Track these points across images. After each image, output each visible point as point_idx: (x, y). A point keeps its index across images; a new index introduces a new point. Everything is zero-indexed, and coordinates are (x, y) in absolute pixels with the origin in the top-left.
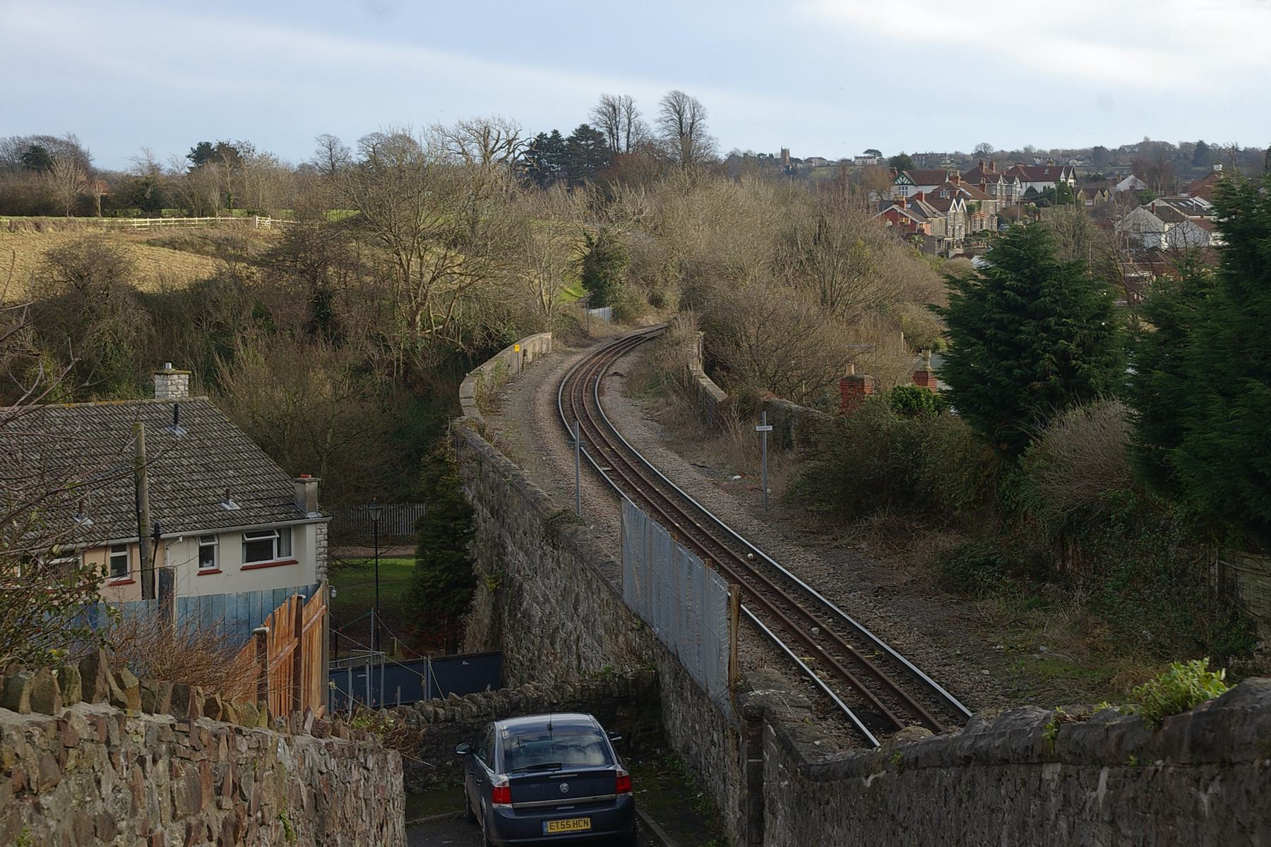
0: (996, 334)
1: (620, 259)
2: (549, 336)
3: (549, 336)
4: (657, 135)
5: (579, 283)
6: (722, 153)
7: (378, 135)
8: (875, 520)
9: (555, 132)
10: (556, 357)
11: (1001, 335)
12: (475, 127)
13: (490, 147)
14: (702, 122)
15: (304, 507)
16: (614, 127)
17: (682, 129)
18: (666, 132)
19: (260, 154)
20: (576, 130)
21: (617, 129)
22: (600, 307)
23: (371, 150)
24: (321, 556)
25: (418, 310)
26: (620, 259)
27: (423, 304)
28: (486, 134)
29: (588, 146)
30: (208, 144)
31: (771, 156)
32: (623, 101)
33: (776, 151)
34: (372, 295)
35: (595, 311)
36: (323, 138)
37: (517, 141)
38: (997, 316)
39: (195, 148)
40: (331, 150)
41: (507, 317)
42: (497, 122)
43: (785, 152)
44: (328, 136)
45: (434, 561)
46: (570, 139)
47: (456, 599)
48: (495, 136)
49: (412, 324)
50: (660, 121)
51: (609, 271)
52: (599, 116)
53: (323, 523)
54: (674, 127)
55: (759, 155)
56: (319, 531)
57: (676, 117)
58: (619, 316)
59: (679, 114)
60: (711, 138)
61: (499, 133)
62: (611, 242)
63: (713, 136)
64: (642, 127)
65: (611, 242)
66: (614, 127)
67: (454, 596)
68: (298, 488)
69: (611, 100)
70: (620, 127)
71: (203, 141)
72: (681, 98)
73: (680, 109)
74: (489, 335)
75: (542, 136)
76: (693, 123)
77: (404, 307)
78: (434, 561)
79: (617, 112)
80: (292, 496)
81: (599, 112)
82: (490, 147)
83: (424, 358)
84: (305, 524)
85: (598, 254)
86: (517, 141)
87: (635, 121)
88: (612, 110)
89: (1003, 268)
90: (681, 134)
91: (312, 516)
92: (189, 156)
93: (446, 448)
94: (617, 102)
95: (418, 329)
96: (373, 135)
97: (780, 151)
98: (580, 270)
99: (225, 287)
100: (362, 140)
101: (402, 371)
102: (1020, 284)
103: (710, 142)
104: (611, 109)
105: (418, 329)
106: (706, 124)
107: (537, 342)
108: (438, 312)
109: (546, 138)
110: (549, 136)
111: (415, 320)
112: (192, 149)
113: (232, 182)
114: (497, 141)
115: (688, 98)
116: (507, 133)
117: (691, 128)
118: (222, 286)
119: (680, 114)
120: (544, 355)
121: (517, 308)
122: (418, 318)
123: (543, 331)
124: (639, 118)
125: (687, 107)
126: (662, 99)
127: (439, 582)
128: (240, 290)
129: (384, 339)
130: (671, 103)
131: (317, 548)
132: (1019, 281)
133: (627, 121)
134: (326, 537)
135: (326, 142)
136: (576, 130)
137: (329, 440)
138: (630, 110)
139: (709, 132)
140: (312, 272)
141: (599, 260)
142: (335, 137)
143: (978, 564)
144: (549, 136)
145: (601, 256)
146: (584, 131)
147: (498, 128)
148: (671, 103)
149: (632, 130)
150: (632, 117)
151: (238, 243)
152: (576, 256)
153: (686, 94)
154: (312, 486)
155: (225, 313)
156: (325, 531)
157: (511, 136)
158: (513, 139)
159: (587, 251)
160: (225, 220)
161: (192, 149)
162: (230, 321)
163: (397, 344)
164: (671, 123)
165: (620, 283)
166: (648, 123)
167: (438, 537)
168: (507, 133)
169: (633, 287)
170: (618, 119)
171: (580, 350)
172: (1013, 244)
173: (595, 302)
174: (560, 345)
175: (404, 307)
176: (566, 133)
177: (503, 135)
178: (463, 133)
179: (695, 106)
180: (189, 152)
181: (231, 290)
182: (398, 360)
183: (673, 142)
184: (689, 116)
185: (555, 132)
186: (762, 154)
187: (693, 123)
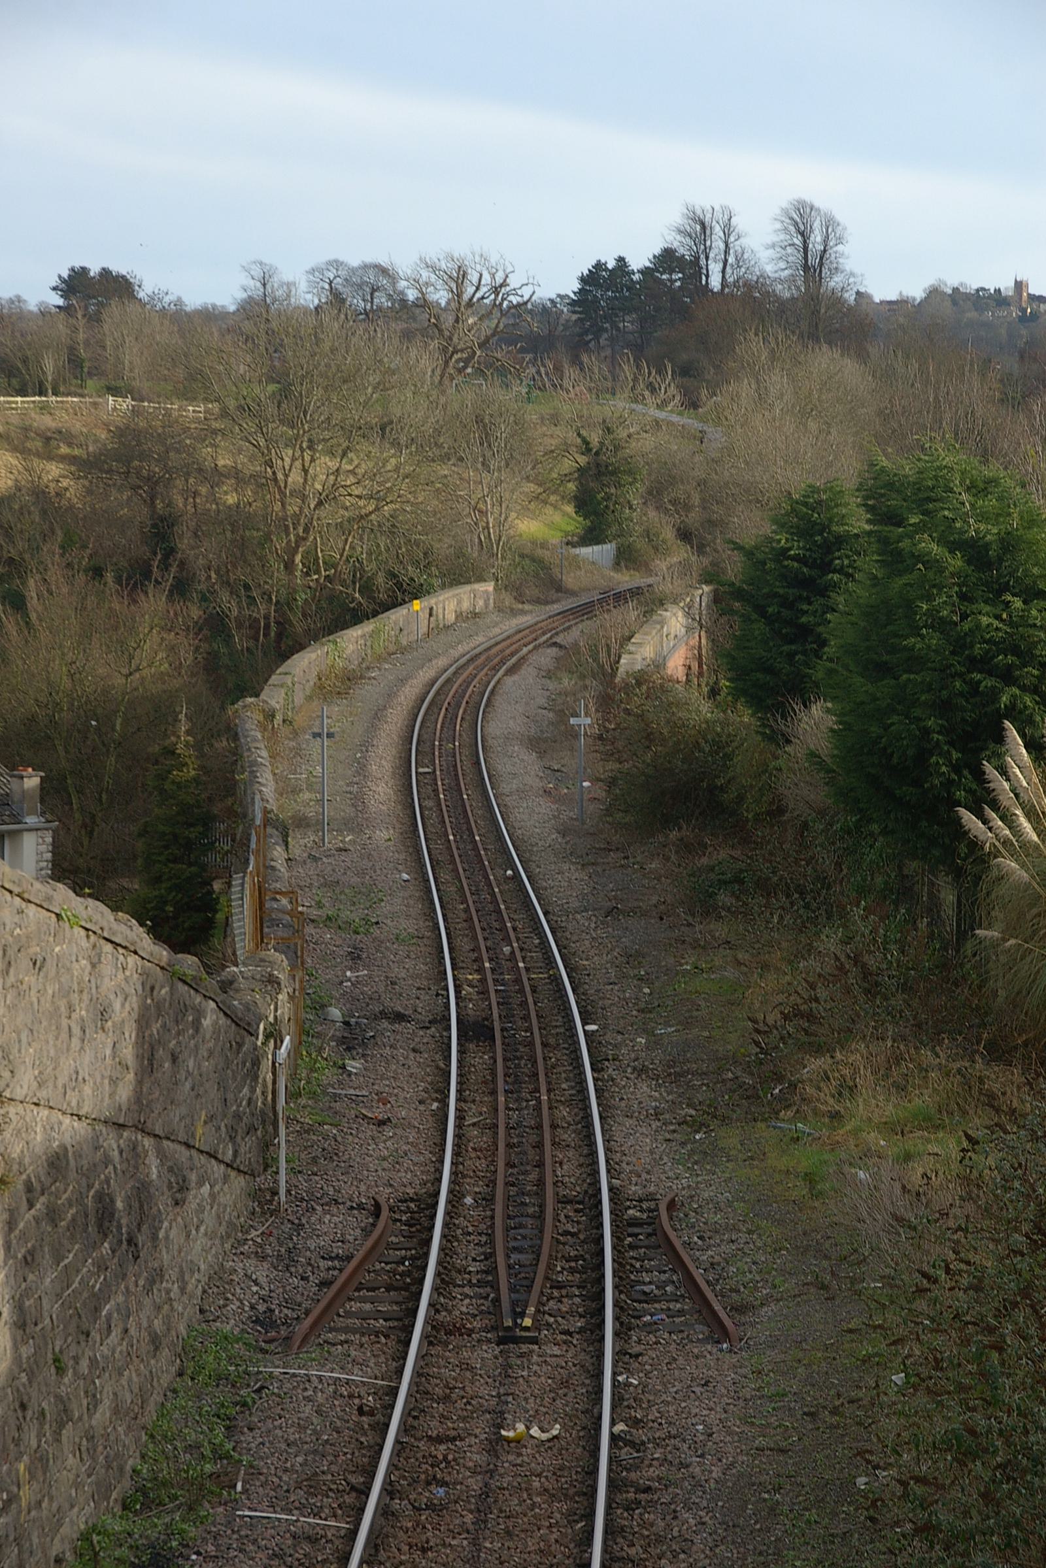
0: (779, 612)
1: (630, 472)
2: (489, 587)
3: (489, 587)
4: (769, 269)
5: (570, 509)
6: (877, 301)
7: (337, 264)
8: (674, 835)
9: (621, 260)
10: (495, 617)
11: (786, 613)
12: (444, 267)
13: (466, 297)
14: (840, 248)
15: (22, 809)
16: (702, 257)
17: (806, 261)
18: (782, 265)
19: (150, 293)
20: (655, 257)
21: (707, 258)
22: (597, 543)
23: (327, 286)
24: (43, 872)
25: (298, 547)
26: (630, 472)
27: (304, 539)
28: (460, 277)
29: (672, 281)
30: (84, 271)
31: (998, 291)
32: (718, 215)
33: (1006, 285)
34: (236, 519)
35: (586, 551)
36: (253, 267)
37: (508, 289)
38: (781, 591)
39: (65, 275)
40: (264, 285)
41: (426, 561)
42: (477, 259)
43: (1019, 285)
44: (261, 263)
45: (160, 877)
46: (645, 272)
47: (186, 925)
48: (475, 280)
49: (289, 566)
50: (773, 246)
51: (613, 490)
52: (678, 237)
53: (47, 829)
54: (796, 257)
55: (978, 291)
56: (40, 840)
57: (798, 241)
58: (626, 558)
59: (802, 234)
60: (852, 274)
61: (481, 275)
62: (617, 448)
63: (857, 270)
64: (746, 256)
65: (617, 448)
66: (702, 257)
67: (184, 922)
68: (15, 784)
69: (699, 212)
70: (712, 255)
71: (77, 264)
72: (808, 210)
73: (806, 228)
74: (399, 585)
75: (599, 266)
76: (825, 251)
77: (279, 544)
78: (160, 877)
79: (708, 232)
80: (7, 795)
81: (680, 232)
82: (466, 297)
83: (304, 615)
84: (21, 831)
85: (598, 465)
86: (508, 289)
87: (735, 246)
88: (699, 228)
89: (792, 534)
90: (806, 268)
91: (31, 820)
92: (55, 289)
93: (179, 737)
94: (709, 216)
95: (298, 574)
96: (330, 263)
97: (1012, 284)
98: (571, 486)
99: (21, 508)
100: (312, 271)
101: (273, 634)
102: (808, 554)
103: (851, 280)
104: (698, 228)
105: (298, 574)
106: (846, 253)
107: (465, 597)
108: (330, 547)
109: (606, 269)
110: (611, 264)
111: (293, 561)
112: (60, 277)
113: (87, 343)
114: (478, 288)
115: (818, 210)
116: (493, 276)
117: (821, 258)
118: (16, 507)
119: (804, 236)
120: (476, 615)
121: (443, 547)
122: (298, 558)
123: (481, 579)
124: (742, 241)
125: (816, 225)
126: (778, 211)
127: (165, 903)
128: (44, 512)
129: (247, 587)
130: (792, 219)
131: (37, 862)
132: (810, 550)
133: (722, 246)
134: (50, 848)
135: (258, 272)
136: (655, 257)
137: (118, 728)
138: (728, 230)
139: (848, 265)
140: (152, 487)
141: (599, 474)
142: (271, 266)
143: (725, 883)
144: (611, 264)
145: (603, 469)
146: (667, 258)
147: (478, 268)
148: (792, 219)
149: (731, 260)
150: (732, 239)
151: (75, 437)
152: (567, 465)
153: (816, 204)
154: (32, 781)
155: (20, 545)
156: (49, 840)
157: (499, 280)
158: (501, 286)
159: (583, 460)
160: (62, 402)
161: (60, 277)
162: (27, 556)
163: (267, 595)
164: (789, 250)
165: (631, 508)
166: (755, 249)
167: (166, 847)
168: (493, 276)
169: (652, 514)
170: (708, 243)
171: (537, 608)
172: (806, 504)
173: (592, 536)
174: (508, 599)
175: (279, 544)
176: (639, 261)
177: (486, 278)
178: (425, 275)
179: (830, 224)
180: (55, 281)
181: (29, 513)
182: (267, 617)
183: (792, 279)
184: (819, 239)
185: (621, 260)
186: (983, 289)
187: (825, 251)
